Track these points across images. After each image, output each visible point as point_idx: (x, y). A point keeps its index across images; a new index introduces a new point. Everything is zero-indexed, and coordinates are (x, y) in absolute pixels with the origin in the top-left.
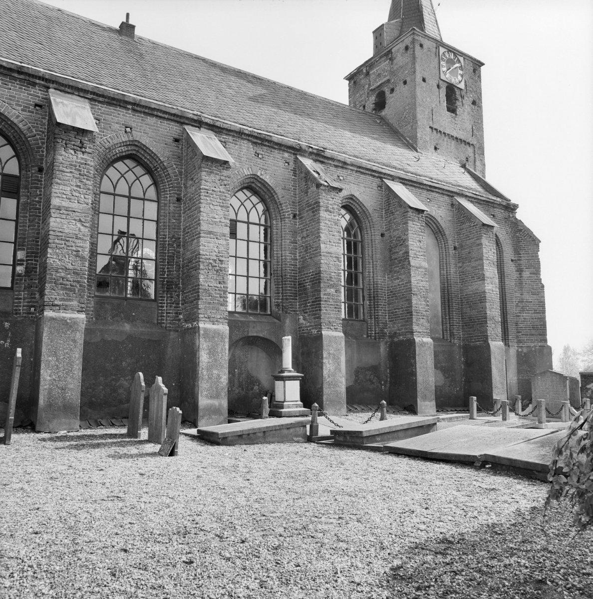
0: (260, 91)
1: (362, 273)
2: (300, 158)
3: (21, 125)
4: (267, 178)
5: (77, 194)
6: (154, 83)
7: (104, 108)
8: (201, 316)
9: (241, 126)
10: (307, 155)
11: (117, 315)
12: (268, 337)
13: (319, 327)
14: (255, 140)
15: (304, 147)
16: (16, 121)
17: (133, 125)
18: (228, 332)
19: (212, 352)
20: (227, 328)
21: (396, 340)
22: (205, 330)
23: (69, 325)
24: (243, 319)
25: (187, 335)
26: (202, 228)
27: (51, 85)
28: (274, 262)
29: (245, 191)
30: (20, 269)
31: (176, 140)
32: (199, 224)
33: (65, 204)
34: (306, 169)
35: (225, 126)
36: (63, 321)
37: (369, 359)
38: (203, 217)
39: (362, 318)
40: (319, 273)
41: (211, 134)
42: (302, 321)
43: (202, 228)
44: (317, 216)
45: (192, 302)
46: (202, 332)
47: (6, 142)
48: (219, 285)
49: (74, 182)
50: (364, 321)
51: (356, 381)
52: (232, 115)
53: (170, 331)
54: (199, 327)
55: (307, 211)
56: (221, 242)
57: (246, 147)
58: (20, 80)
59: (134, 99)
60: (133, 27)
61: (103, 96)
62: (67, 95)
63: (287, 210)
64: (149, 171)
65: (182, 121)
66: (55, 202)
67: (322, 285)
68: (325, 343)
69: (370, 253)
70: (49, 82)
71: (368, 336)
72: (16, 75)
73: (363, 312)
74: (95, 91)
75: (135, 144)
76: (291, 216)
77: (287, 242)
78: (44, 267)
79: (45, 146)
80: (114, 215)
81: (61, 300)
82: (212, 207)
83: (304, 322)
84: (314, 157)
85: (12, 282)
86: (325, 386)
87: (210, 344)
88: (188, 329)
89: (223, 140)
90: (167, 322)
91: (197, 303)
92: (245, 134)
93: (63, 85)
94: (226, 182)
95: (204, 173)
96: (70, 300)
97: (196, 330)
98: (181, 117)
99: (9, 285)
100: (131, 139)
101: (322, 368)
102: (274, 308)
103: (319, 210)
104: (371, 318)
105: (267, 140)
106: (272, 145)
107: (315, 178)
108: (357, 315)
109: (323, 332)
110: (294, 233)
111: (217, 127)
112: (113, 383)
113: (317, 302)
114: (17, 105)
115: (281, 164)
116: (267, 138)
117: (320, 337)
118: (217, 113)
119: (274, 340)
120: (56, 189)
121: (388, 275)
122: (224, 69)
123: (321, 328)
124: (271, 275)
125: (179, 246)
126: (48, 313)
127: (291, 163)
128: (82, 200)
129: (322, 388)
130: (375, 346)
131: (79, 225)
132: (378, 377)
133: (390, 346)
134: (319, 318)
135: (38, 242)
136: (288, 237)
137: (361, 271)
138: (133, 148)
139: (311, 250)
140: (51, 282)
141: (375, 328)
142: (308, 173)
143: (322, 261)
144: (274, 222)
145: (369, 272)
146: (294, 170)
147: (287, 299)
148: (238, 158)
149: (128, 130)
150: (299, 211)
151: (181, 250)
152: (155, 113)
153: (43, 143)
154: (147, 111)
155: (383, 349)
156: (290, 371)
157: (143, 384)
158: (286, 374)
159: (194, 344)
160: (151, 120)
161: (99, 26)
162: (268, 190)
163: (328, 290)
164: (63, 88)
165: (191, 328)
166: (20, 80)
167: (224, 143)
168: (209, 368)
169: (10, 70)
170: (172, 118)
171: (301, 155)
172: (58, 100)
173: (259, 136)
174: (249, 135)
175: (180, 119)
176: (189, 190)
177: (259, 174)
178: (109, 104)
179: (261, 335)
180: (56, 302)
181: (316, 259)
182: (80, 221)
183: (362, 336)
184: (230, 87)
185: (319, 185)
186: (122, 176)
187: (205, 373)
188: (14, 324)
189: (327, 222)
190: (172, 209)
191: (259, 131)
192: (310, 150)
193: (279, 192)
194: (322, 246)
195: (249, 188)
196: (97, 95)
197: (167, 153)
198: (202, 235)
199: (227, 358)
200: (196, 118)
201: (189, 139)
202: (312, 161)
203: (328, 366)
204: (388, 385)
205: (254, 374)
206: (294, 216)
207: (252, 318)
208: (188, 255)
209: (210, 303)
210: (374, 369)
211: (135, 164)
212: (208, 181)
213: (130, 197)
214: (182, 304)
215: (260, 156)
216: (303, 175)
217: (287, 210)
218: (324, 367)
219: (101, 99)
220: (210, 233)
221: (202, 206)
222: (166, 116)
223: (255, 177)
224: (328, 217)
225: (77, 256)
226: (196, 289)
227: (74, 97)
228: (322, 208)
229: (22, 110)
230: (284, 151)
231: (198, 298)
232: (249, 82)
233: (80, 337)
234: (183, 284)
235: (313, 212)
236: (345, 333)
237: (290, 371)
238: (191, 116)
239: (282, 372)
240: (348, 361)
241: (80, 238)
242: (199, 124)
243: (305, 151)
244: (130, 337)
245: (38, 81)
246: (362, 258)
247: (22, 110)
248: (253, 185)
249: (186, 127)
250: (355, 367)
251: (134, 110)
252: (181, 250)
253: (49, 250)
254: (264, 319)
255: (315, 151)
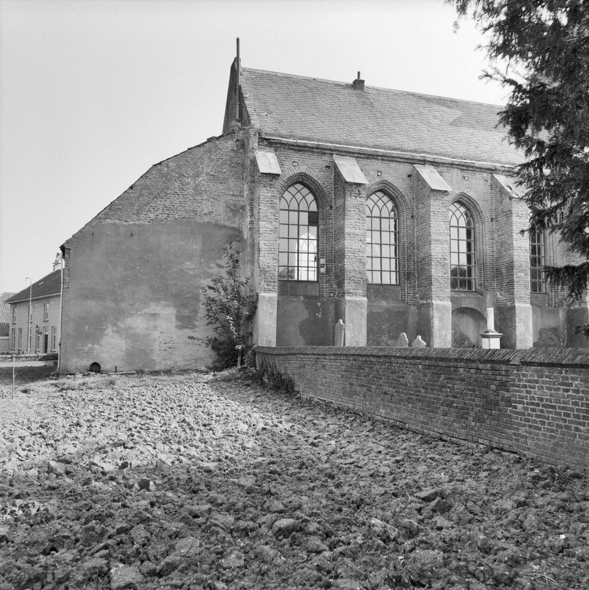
0: (459, 113)
1: (544, 257)
2: (496, 176)
3: (319, 181)
4: (471, 194)
5: (358, 224)
6: (386, 129)
7: (365, 162)
8: (433, 296)
9: (453, 159)
10: (500, 172)
11: (377, 296)
12: (475, 308)
13: (512, 300)
14: (463, 168)
15: (498, 168)
16: (316, 179)
17: (382, 170)
18: (451, 306)
19: (441, 319)
20: (451, 303)
21: (572, 308)
22: (437, 305)
23: (358, 304)
24: (457, 296)
25: (423, 308)
26: (432, 238)
27: (334, 153)
28: (477, 254)
29: (455, 204)
30: (323, 270)
31: (409, 176)
32: (430, 235)
33: (352, 231)
34: (501, 185)
35: (442, 161)
36: (355, 302)
37: (550, 322)
38: (433, 230)
39: (544, 291)
40: (513, 262)
41: (432, 168)
42: (499, 296)
43: (432, 238)
44: (510, 221)
45: (426, 286)
46: (434, 307)
47: (303, 187)
48: (444, 275)
49: (357, 216)
50: (546, 293)
51: (540, 339)
52: (441, 145)
53: (410, 305)
54: (432, 303)
55: (502, 216)
56: (444, 246)
57: (456, 173)
58: (317, 152)
59: (382, 152)
60: (363, 82)
61: (364, 154)
62: (343, 157)
63: (487, 215)
64: (392, 199)
65: (413, 162)
66: (347, 230)
67: (515, 271)
68: (517, 311)
69: (551, 242)
70: (332, 151)
71: (549, 305)
72: (315, 150)
73: (545, 287)
74: (360, 152)
75: (384, 182)
76: (490, 220)
77: (487, 239)
78: (343, 270)
79: (333, 192)
80: (372, 231)
81: (354, 289)
82: (438, 223)
83: (501, 297)
84: (506, 173)
85: (318, 278)
86: (518, 342)
87: (440, 314)
88: (423, 304)
89: (440, 171)
90: (408, 299)
91: (430, 288)
92: (455, 164)
93: (341, 151)
94: (446, 205)
95: (432, 200)
96: (358, 289)
97: (430, 305)
98: (412, 159)
99: (316, 280)
100: (381, 179)
101: (515, 330)
102: (478, 287)
103: (511, 216)
104: (552, 292)
105: (472, 167)
106: (474, 169)
107: (508, 193)
108: (540, 290)
109: (516, 304)
110: (492, 232)
111: (436, 162)
112: (378, 339)
113: (511, 283)
114: (316, 168)
115: (482, 182)
116: (471, 165)
117: (513, 308)
118: (431, 146)
119: (479, 310)
120: (347, 222)
121: (566, 258)
122: (429, 100)
123: (514, 302)
124: (475, 263)
125: (414, 248)
126: (347, 298)
127: (489, 180)
128: (361, 227)
129: (515, 343)
130: (555, 313)
131: (360, 243)
132: (558, 336)
133: (568, 312)
134: (513, 294)
135: (332, 253)
136: (488, 235)
137: (543, 255)
138: (383, 185)
139: (505, 245)
140: (347, 279)
141: (555, 299)
142: (502, 188)
143: (514, 254)
144: (477, 225)
145: (550, 256)
146: (491, 185)
147: (487, 281)
148: (451, 183)
149: (379, 173)
150: (496, 216)
151: (416, 251)
152: (396, 159)
153: (332, 191)
154: (390, 159)
155: (562, 315)
156: (493, 332)
157: (407, 340)
158: (490, 334)
159: (429, 314)
160: (393, 165)
161: (339, 85)
162: (472, 202)
163: (519, 274)
164: (340, 153)
165: (426, 304)
166: (317, 152)
167: (441, 173)
168: (440, 330)
169: (313, 148)
170: (406, 161)
171: (496, 173)
172: (340, 162)
173: (465, 164)
174: (458, 165)
175: (411, 161)
176: (420, 210)
177: (465, 192)
178: (367, 158)
179: (470, 306)
180: (351, 291)
181: (510, 252)
182: (361, 240)
183: (544, 305)
184: (435, 117)
185: (511, 198)
186: (376, 204)
187: (437, 333)
188: (322, 304)
189: (518, 225)
190: (408, 223)
191: (465, 161)
192: (503, 169)
193: (481, 203)
194: (515, 242)
195: (459, 202)
196: (361, 154)
197: (404, 186)
198: (432, 242)
199: (451, 323)
200: (422, 159)
201: (418, 175)
202: (504, 177)
203: (520, 328)
204: (566, 342)
205: (465, 333)
206: (492, 220)
207: (463, 295)
208: (422, 255)
209: (438, 287)
210: (555, 330)
211: (382, 195)
212: (435, 205)
213: (381, 218)
214: (418, 287)
215: (466, 179)
216: (498, 189)
217: (487, 215)
218: (517, 329)
219: (363, 156)
220: (438, 240)
221: (431, 223)
222: (403, 160)
223: (463, 195)
224: (518, 220)
225: (360, 262)
226: (429, 278)
227: (347, 157)
228: (514, 215)
229: (320, 171)
230: (483, 172)
231: (431, 284)
232: (449, 107)
233: (365, 311)
234: (418, 274)
235: (507, 217)
236: (531, 304)
237: (493, 332)
238: (419, 158)
239: (487, 332)
240: (535, 324)
241: (361, 252)
242: (424, 162)
243: (499, 170)
244: (387, 310)
245: (327, 152)
246: (544, 245)
247: (320, 171)
248: (461, 200)
249: (415, 165)
250: (539, 328)
251: (382, 160)
252: (416, 251)
253: (346, 260)
254: (470, 295)
255: (507, 169)
